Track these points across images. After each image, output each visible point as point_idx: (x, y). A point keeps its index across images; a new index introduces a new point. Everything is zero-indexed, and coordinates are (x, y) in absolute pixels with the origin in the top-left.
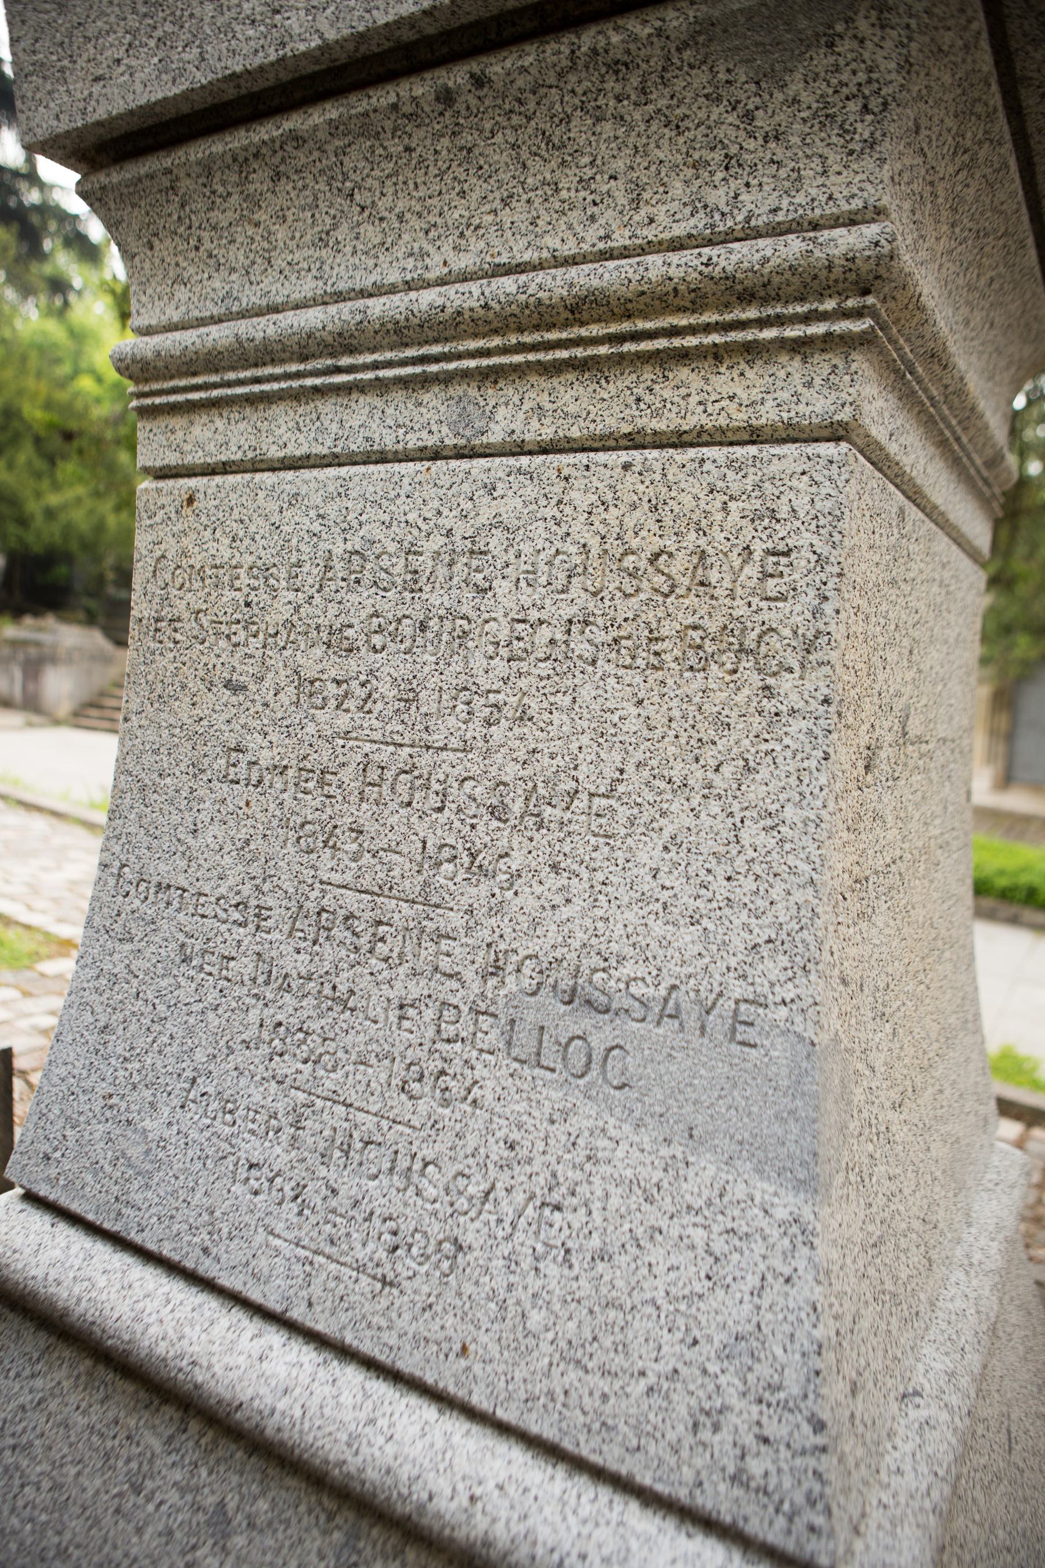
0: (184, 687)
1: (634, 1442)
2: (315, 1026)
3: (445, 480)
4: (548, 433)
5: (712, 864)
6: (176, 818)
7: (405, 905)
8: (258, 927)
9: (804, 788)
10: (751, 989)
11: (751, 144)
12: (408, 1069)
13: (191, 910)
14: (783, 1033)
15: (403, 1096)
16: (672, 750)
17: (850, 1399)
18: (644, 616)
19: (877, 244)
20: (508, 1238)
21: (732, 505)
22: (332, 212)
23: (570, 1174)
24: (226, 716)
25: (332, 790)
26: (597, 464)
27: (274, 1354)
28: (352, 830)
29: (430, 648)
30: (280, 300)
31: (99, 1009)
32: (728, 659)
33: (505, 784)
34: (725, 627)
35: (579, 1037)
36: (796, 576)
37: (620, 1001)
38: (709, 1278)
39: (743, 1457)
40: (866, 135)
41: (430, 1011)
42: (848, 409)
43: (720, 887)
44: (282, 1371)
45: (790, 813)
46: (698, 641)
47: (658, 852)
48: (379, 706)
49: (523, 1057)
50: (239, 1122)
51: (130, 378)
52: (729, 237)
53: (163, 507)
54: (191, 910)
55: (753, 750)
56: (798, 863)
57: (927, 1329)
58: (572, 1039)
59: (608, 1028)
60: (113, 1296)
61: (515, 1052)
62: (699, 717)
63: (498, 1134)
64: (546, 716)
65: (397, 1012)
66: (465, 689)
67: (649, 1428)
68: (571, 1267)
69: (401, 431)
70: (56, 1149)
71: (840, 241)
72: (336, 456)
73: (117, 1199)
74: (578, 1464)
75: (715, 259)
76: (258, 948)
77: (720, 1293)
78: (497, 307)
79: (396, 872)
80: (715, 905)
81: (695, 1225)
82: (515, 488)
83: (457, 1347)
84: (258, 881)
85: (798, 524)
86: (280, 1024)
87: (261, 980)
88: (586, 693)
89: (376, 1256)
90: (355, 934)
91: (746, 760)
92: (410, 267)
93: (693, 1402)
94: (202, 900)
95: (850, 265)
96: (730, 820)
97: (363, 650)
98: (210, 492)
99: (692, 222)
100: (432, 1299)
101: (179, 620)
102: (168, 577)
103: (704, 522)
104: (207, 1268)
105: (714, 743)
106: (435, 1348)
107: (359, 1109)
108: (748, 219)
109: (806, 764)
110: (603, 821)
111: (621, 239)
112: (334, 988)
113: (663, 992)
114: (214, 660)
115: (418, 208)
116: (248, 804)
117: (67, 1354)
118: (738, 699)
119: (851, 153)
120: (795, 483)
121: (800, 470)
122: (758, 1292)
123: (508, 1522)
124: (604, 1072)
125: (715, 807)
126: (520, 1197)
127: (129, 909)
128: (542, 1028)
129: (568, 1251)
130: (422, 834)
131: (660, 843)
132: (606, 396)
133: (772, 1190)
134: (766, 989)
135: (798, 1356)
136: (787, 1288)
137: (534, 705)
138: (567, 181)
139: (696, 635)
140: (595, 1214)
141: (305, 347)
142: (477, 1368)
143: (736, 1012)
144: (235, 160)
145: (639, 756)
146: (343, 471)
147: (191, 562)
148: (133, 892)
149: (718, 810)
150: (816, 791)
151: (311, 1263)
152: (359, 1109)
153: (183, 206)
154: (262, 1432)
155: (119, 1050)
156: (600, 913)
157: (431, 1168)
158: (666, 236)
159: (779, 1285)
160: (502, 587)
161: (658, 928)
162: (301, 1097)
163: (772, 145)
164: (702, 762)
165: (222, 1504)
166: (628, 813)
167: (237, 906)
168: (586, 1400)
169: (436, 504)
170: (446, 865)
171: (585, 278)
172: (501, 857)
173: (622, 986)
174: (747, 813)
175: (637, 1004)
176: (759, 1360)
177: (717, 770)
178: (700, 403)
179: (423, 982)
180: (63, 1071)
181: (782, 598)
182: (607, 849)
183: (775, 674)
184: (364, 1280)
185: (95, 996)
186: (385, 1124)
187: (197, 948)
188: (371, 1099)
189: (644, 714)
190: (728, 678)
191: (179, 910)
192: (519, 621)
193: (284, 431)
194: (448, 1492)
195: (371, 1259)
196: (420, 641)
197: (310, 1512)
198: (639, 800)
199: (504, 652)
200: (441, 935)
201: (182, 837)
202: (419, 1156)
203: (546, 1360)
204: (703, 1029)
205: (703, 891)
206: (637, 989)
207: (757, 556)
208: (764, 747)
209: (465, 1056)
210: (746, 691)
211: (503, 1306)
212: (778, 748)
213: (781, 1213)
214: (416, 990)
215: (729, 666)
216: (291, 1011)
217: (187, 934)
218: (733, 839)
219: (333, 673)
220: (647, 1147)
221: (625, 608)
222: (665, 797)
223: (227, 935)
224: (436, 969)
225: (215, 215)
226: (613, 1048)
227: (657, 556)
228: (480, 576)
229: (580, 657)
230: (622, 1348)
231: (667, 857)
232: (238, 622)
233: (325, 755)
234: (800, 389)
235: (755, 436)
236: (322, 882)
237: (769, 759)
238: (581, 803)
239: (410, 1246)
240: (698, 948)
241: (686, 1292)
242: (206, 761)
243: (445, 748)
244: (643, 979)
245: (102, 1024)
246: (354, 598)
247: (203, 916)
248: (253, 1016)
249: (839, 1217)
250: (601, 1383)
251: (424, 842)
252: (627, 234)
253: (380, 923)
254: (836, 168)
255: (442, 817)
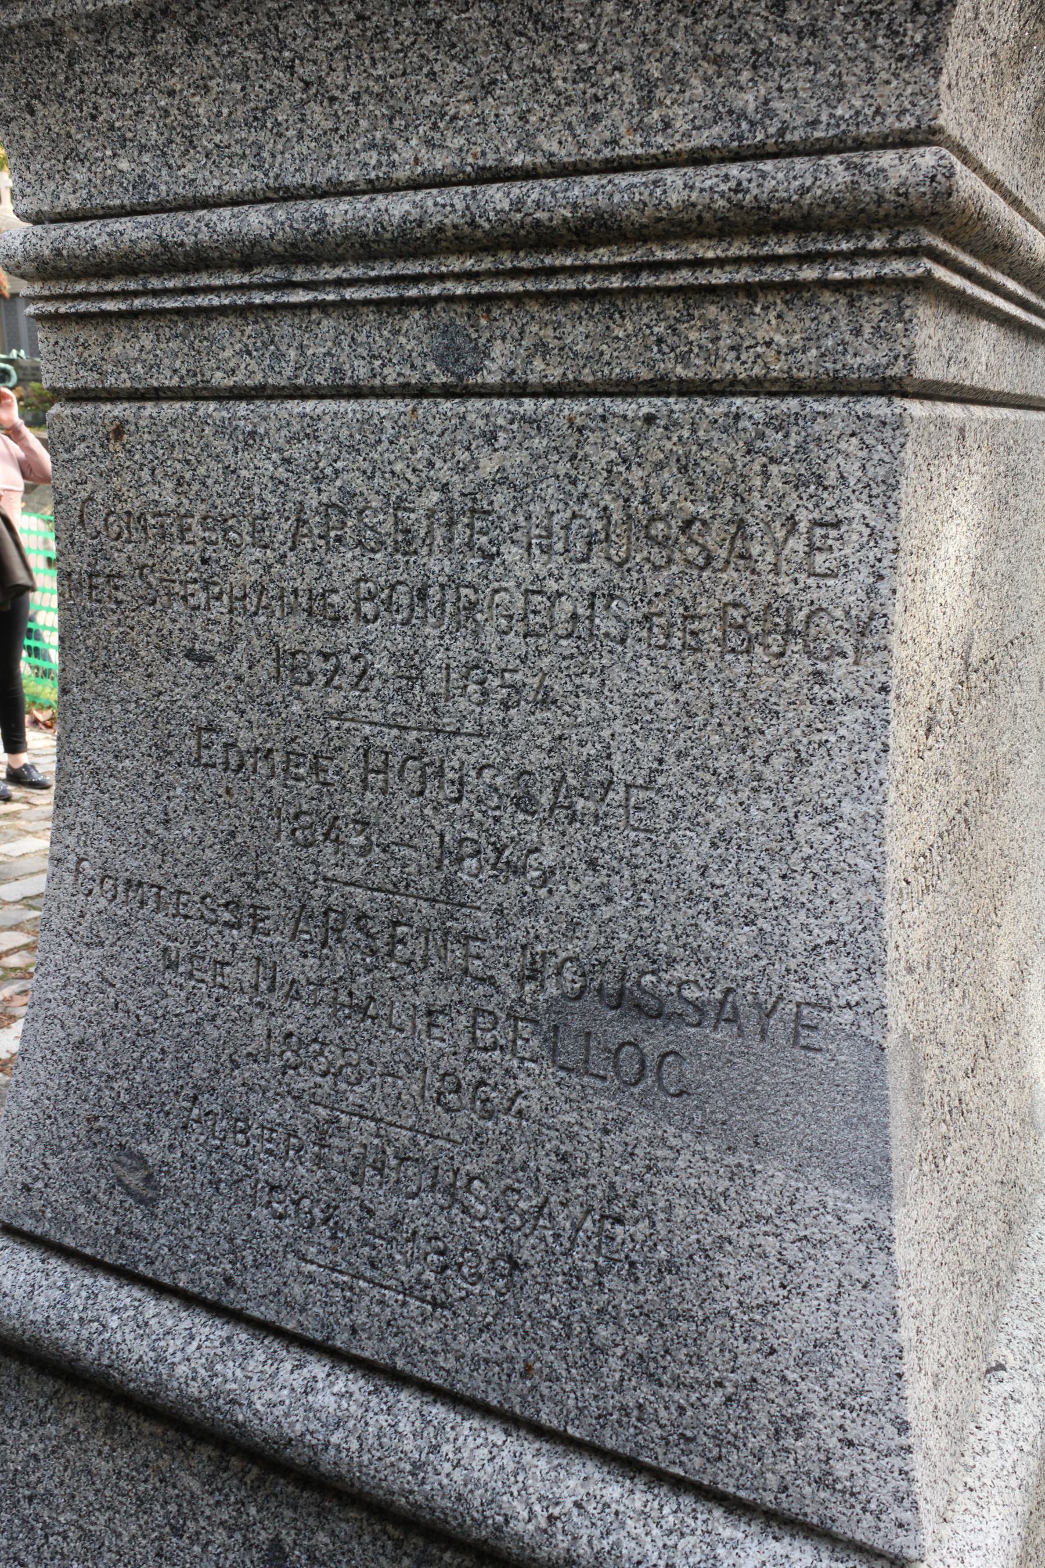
0: (134, 654)
1: (715, 1452)
2: (333, 1035)
3: (436, 425)
4: (554, 375)
5: (765, 861)
6: (142, 807)
7: (425, 904)
8: (254, 929)
9: (862, 781)
10: (813, 992)
11: (784, 40)
12: (442, 1080)
13: (172, 910)
14: (849, 1037)
15: (439, 1109)
16: (715, 739)
17: (933, 1394)
18: (677, 592)
19: (933, 179)
20: (567, 1253)
21: (773, 469)
22: (268, 86)
23: (629, 1185)
24: (191, 690)
25: (330, 776)
26: (614, 415)
27: (320, 1385)
28: (356, 822)
29: (432, 620)
30: (210, 191)
31: (69, 1022)
32: (775, 641)
33: (530, 773)
34: (770, 606)
35: (630, 1043)
36: (847, 551)
37: (674, 1006)
38: (784, 1287)
39: (827, 1461)
40: (918, 38)
41: (463, 1018)
42: (901, 362)
43: (776, 887)
44: (330, 1401)
45: (847, 808)
46: (740, 620)
47: (706, 847)
48: (377, 683)
49: (570, 1065)
50: (253, 1142)
51: (23, 276)
52: (760, 153)
53: (83, 438)
54: (172, 910)
55: (805, 741)
56: (859, 861)
57: (660, 647)
58: (622, 1046)
59: (661, 1034)
60: (129, 1337)
61: (562, 1059)
62: (744, 705)
63: (548, 1146)
64: (572, 700)
65: (426, 1020)
66: (477, 667)
67: (730, 1438)
68: (636, 1280)
69: (377, 363)
70: (36, 1179)
71: (891, 173)
72: (297, 388)
73: (118, 1230)
74: (656, 1476)
75: (745, 184)
76: (256, 952)
77: (796, 1301)
78: (487, 226)
79: (412, 868)
80: (770, 904)
81: (766, 1234)
82: (519, 437)
83: (519, 1366)
84: (250, 878)
85: (848, 492)
86: (290, 1035)
87: (264, 986)
88: (618, 675)
89: (424, 1277)
90: (368, 935)
91: (798, 751)
92: (373, 162)
93: (774, 1410)
94: (184, 899)
95: (902, 200)
96: (784, 815)
97: (352, 620)
98: (142, 423)
99: (716, 130)
100: (489, 1319)
101: (119, 576)
102: (99, 524)
103: (741, 488)
104: (232, 1298)
105: (762, 733)
106: (497, 1369)
107: (390, 1124)
108: (782, 132)
109: (863, 756)
110: (642, 815)
111: (631, 146)
112: (351, 994)
113: (719, 996)
114: (169, 626)
115: (377, 89)
116: (228, 791)
117: (79, 1398)
118: (787, 684)
119: (901, 58)
120: (843, 446)
121: (849, 431)
122: (834, 1299)
123: (590, 1542)
124: (659, 1079)
125: (766, 801)
126: (577, 1211)
127: (94, 909)
128: (589, 1034)
129: (632, 1264)
130: (438, 827)
131: (707, 838)
132: (621, 334)
133: (844, 1196)
134: (829, 992)
135: (879, 1361)
136: (865, 1294)
137: (558, 686)
138: (561, 68)
139: (737, 614)
140: (659, 1226)
141: (249, 255)
142: (544, 1388)
143: (798, 1015)
144: (137, 15)
145: (680, 745)
146: (309, 406)
147: (128, 507)
148: (97, 890)
149: (768, 804)
150: (876, 785)
151: (351, 1289)
152: (390, 1124)
153: (71, 65)
154: (316, 1468)
155: (101, 1067)
156: (646, 912)
157: (476, 1184)
158: (687, 145)
159: (857, 1292)
160: (512, 553)
161: (709, 928)
162: (323, 1112)
163: (808, 42)
164: (749, 753)
165: (276, 1543)
166: (670, 806)
167: (226, 905)
168: (663, 1413)
169: (426, 453)
170: (467, 862)
171: (588, 191)
172: (531, 852)
173: (674, 989)
174: (801, 808)
175: (690, 1009)
176: (839, 1366)
177: (766, 761)
178: (732, 348)
179: (452, 988)
180: (33, 1092)
181: (832, 574)
182: (647, 845)
183: (826, 658)
184: (414, 1303)
185: (63, 1009)
186: (421, 1140)
187: (183, 953)
188: (404, 1113)
189: (682, 700)
190: (775, 662)
191: (157, 911)
192: (534, 592)
193: (231, 355)
194: (525, 1514)
195: (418, 1281)
196: (419, 611)
197: (375, 1539)
198: (682, 793)
199: (520, 627)
200: (466, 938)
201: (150, 827)
202: (463, 1172)
203: (617, 1375)
204: (763, 1033)
205: (757, 890)
206: (688, 993)
207: (803, 527)
208: (817, 737)
209: (506, 1065)
210: (795, 677)
211: (567, 1325)
212: (833, 739)
213: (855, 1220)
214: (443, 996)
215: (775, 649)
216: (301, 1018)
217: (169, 938)
218: (786, 835)
219: (318, 645)
220: (711, 1156)
221: (657, 584)
222: (711, 789)
223: (218, 938)
224: (466, 971)
225: (116, 79)
226: (667, 1054)
227: (688, 523)
228: (484, 539)
229: (607, 635)
230: (697, 1360)
231: (715, 853)
232: (195, 581)
233: (317, 738)
234: (848, 337)
235: (795, 388)
236: (325, 879)
237: (823, 751)
238: (616, 796)
239: (460, 1266)
240: (754, 950)
241: (761, 1301)
242: (172, 743)
243: (457, 733)
244: (696, 982)
245: (76, 1038)
246: (335, 560)
247: (186, 917)
248: (259, 1026)
249: (914, 1214)
250: (676, 1396)
251: (442, 836)
252: (639, 140)
253: (397, 924)
254: (884, 75)
255: (459, 809)
